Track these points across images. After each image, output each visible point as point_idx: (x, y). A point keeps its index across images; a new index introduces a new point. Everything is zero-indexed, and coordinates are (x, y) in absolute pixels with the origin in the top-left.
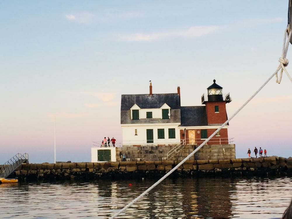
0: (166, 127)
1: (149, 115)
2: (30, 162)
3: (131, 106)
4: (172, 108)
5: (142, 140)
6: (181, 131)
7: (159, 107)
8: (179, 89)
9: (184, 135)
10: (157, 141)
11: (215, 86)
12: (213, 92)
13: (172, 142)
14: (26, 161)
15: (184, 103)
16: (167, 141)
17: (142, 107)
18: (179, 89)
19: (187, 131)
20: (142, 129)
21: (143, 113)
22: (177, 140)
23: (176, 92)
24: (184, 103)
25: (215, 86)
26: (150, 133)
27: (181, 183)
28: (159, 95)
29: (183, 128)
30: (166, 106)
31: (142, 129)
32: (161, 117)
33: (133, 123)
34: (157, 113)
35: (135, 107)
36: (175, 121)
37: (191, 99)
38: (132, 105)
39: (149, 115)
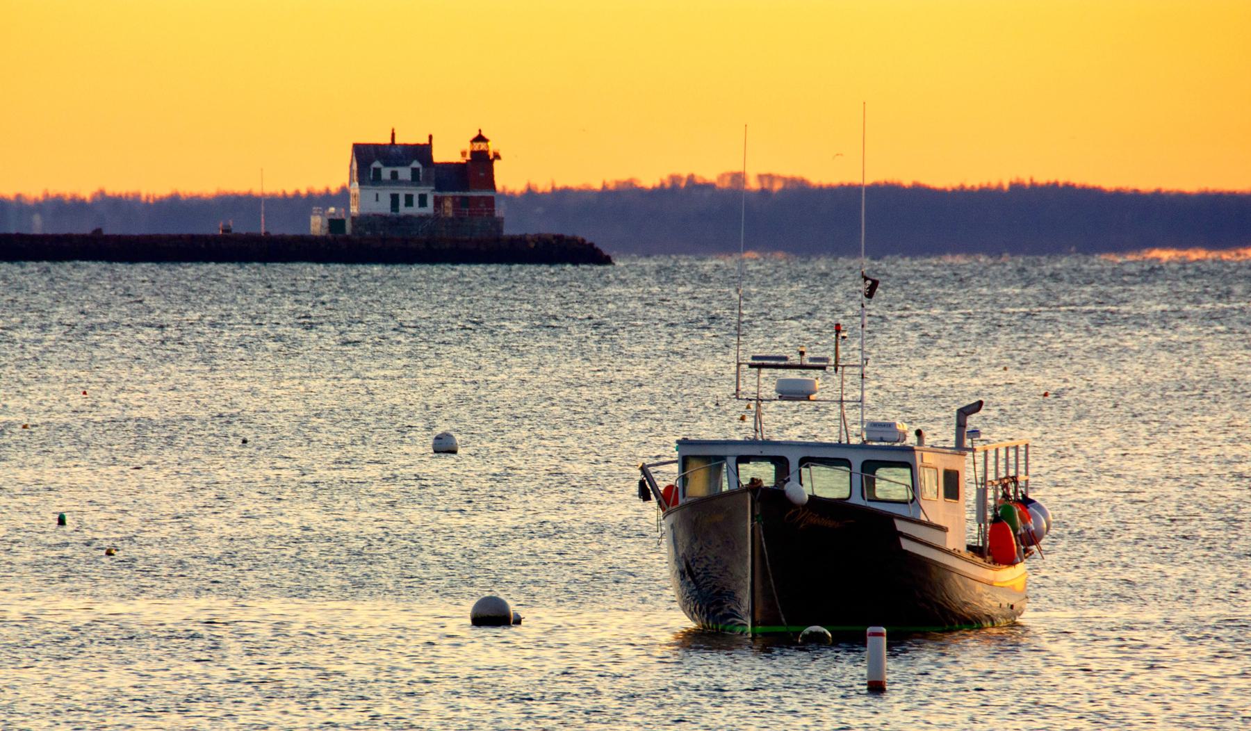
0: (416, 192)
1: (394, 175)
2: (234, 231)
3: (369, 159)
4: (424, 166)
5: (384, 207)
6: (436, 197)
7: (407, 165)
8: (431, 137)
9: (438, 202)
10: (403, 210)
11: (480, 138)
12: (477, 146)
13: (423, 211)
14: (102, 193)
15: (439, 156)
16: (415, 210)
17: (386, 165)
18: (431, 137)
19: (443, 198)
20: (385, 195)
21: (386, 173)
22: (430, 209)
23: (426, 141)
24: (439, 156)
25: (480, 138)
26: (395, 198)
27: (1040, 493)
28: (405, 145)
29: (439, 194)
30: (416, 164)
31: (385, 195)
32: (409, 177)
33: (373, 185)
34: (405, 173)
35: (377, 164)
36: (428, 185)
37: (448, 152)
38: (372, 161)
39: (394, 175)
